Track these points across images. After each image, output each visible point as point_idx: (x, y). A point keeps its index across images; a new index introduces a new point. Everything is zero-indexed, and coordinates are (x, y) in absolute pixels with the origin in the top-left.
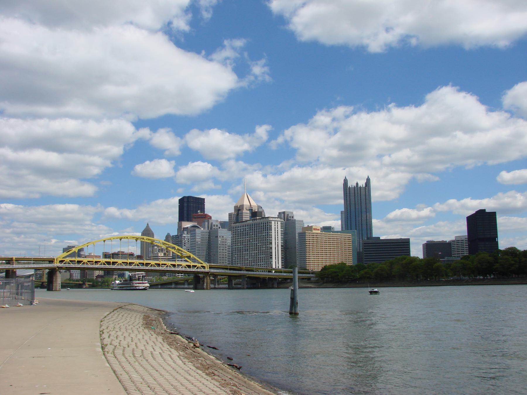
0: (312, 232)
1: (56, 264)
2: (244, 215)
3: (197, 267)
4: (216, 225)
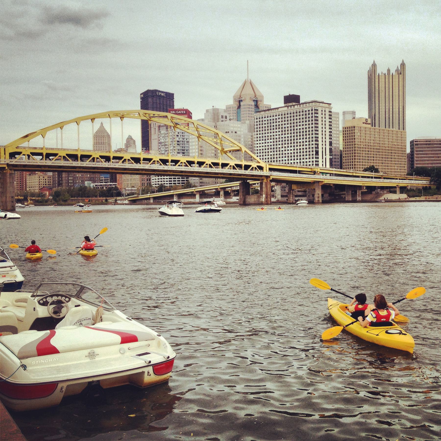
3: (251, 168)
4: (224, 117)
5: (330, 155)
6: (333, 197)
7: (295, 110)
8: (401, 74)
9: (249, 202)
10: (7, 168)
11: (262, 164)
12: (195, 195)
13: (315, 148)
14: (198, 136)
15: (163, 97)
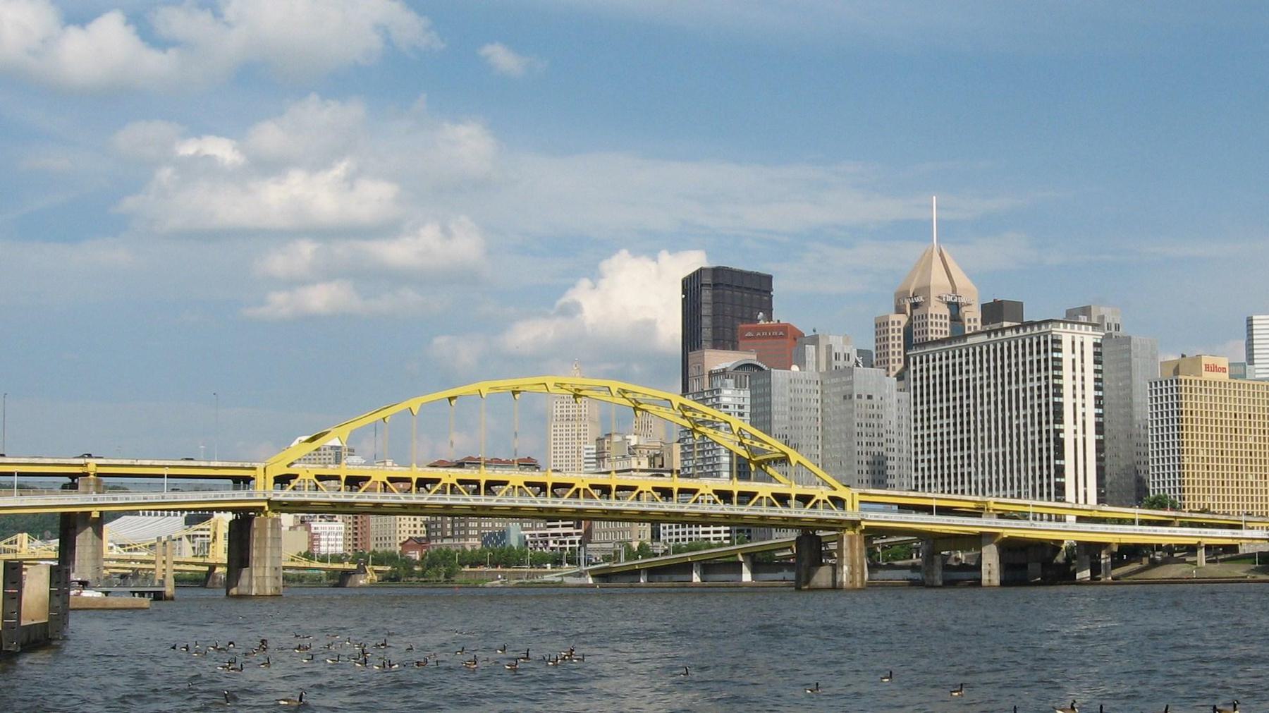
0: (1198, 379)
1: (264, 490)
2: (932, 323)
9: (816, 583)
10: (267, 508)
11: (842, 492)
12: (737, 567)
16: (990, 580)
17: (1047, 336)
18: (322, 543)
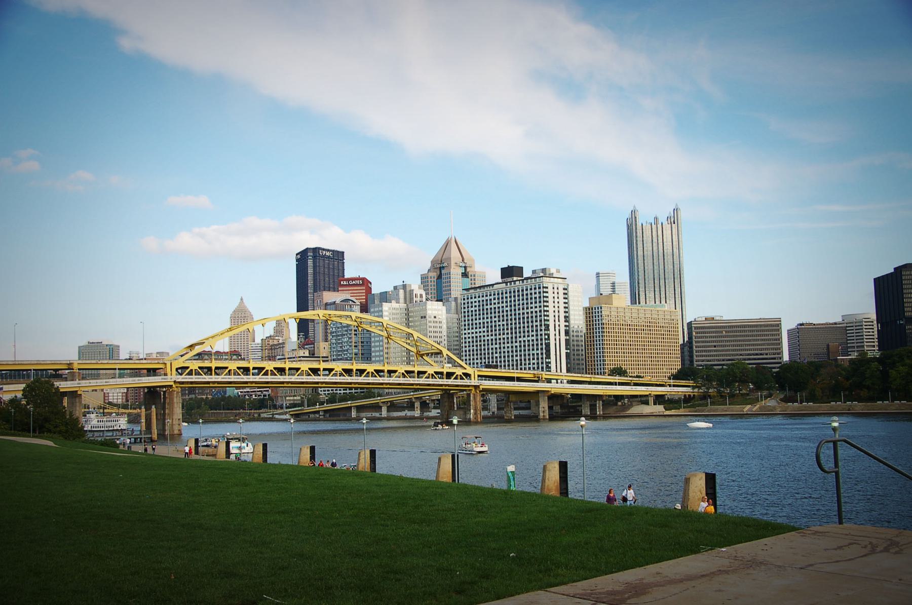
3: (455, 376)
4: (419, 295)
5: (566, 349)
6: (566, 410)
7: (516, 288)
8: (674, 223)
10: (174, 386)
11: (469, 370)
13: (545, 339)
14: (387, 336)
15: (329, 257)
16: (544, 416)
17: (535, 285)
18: (110, 398)
